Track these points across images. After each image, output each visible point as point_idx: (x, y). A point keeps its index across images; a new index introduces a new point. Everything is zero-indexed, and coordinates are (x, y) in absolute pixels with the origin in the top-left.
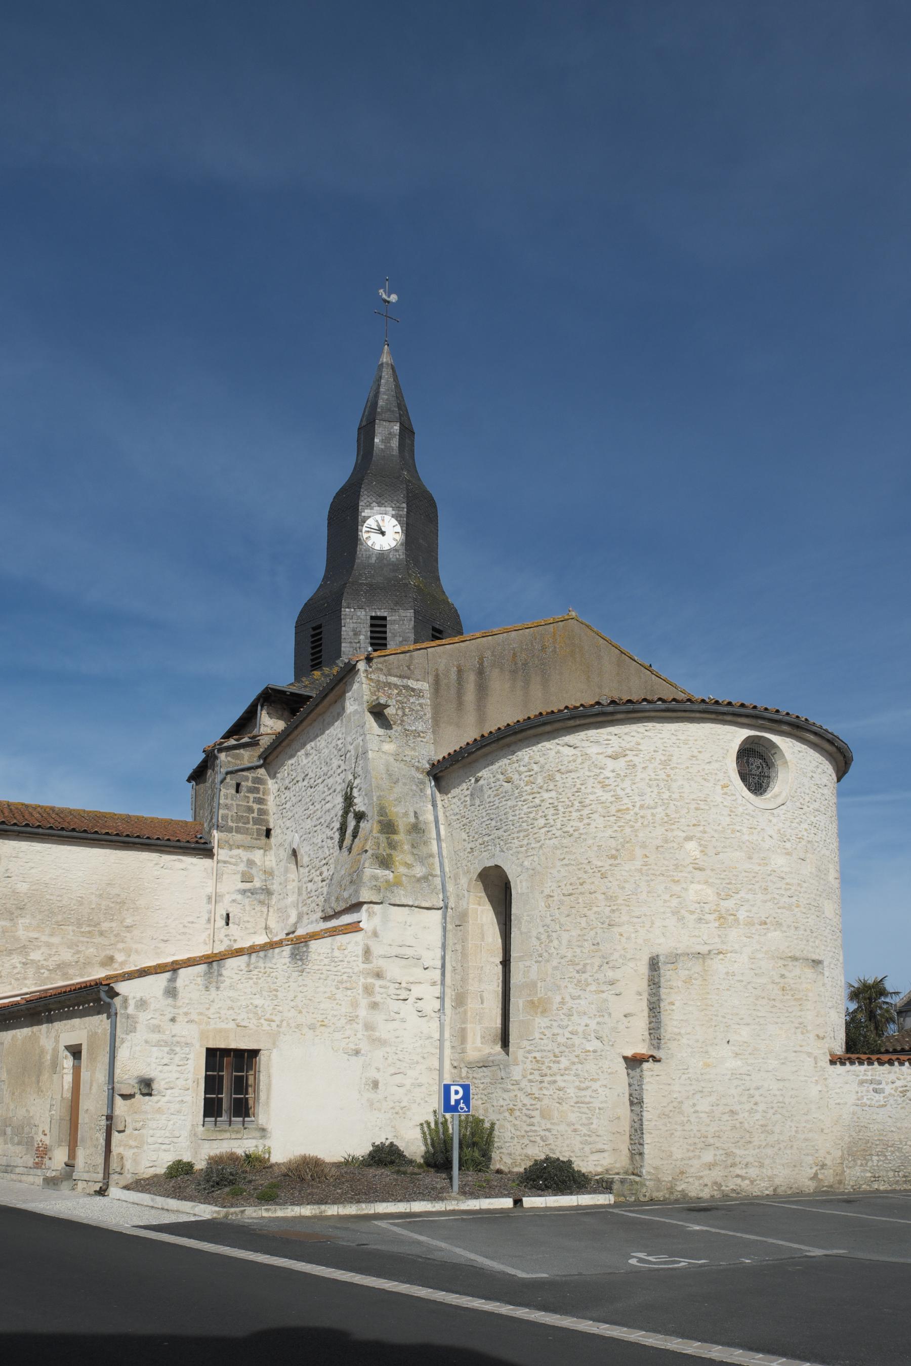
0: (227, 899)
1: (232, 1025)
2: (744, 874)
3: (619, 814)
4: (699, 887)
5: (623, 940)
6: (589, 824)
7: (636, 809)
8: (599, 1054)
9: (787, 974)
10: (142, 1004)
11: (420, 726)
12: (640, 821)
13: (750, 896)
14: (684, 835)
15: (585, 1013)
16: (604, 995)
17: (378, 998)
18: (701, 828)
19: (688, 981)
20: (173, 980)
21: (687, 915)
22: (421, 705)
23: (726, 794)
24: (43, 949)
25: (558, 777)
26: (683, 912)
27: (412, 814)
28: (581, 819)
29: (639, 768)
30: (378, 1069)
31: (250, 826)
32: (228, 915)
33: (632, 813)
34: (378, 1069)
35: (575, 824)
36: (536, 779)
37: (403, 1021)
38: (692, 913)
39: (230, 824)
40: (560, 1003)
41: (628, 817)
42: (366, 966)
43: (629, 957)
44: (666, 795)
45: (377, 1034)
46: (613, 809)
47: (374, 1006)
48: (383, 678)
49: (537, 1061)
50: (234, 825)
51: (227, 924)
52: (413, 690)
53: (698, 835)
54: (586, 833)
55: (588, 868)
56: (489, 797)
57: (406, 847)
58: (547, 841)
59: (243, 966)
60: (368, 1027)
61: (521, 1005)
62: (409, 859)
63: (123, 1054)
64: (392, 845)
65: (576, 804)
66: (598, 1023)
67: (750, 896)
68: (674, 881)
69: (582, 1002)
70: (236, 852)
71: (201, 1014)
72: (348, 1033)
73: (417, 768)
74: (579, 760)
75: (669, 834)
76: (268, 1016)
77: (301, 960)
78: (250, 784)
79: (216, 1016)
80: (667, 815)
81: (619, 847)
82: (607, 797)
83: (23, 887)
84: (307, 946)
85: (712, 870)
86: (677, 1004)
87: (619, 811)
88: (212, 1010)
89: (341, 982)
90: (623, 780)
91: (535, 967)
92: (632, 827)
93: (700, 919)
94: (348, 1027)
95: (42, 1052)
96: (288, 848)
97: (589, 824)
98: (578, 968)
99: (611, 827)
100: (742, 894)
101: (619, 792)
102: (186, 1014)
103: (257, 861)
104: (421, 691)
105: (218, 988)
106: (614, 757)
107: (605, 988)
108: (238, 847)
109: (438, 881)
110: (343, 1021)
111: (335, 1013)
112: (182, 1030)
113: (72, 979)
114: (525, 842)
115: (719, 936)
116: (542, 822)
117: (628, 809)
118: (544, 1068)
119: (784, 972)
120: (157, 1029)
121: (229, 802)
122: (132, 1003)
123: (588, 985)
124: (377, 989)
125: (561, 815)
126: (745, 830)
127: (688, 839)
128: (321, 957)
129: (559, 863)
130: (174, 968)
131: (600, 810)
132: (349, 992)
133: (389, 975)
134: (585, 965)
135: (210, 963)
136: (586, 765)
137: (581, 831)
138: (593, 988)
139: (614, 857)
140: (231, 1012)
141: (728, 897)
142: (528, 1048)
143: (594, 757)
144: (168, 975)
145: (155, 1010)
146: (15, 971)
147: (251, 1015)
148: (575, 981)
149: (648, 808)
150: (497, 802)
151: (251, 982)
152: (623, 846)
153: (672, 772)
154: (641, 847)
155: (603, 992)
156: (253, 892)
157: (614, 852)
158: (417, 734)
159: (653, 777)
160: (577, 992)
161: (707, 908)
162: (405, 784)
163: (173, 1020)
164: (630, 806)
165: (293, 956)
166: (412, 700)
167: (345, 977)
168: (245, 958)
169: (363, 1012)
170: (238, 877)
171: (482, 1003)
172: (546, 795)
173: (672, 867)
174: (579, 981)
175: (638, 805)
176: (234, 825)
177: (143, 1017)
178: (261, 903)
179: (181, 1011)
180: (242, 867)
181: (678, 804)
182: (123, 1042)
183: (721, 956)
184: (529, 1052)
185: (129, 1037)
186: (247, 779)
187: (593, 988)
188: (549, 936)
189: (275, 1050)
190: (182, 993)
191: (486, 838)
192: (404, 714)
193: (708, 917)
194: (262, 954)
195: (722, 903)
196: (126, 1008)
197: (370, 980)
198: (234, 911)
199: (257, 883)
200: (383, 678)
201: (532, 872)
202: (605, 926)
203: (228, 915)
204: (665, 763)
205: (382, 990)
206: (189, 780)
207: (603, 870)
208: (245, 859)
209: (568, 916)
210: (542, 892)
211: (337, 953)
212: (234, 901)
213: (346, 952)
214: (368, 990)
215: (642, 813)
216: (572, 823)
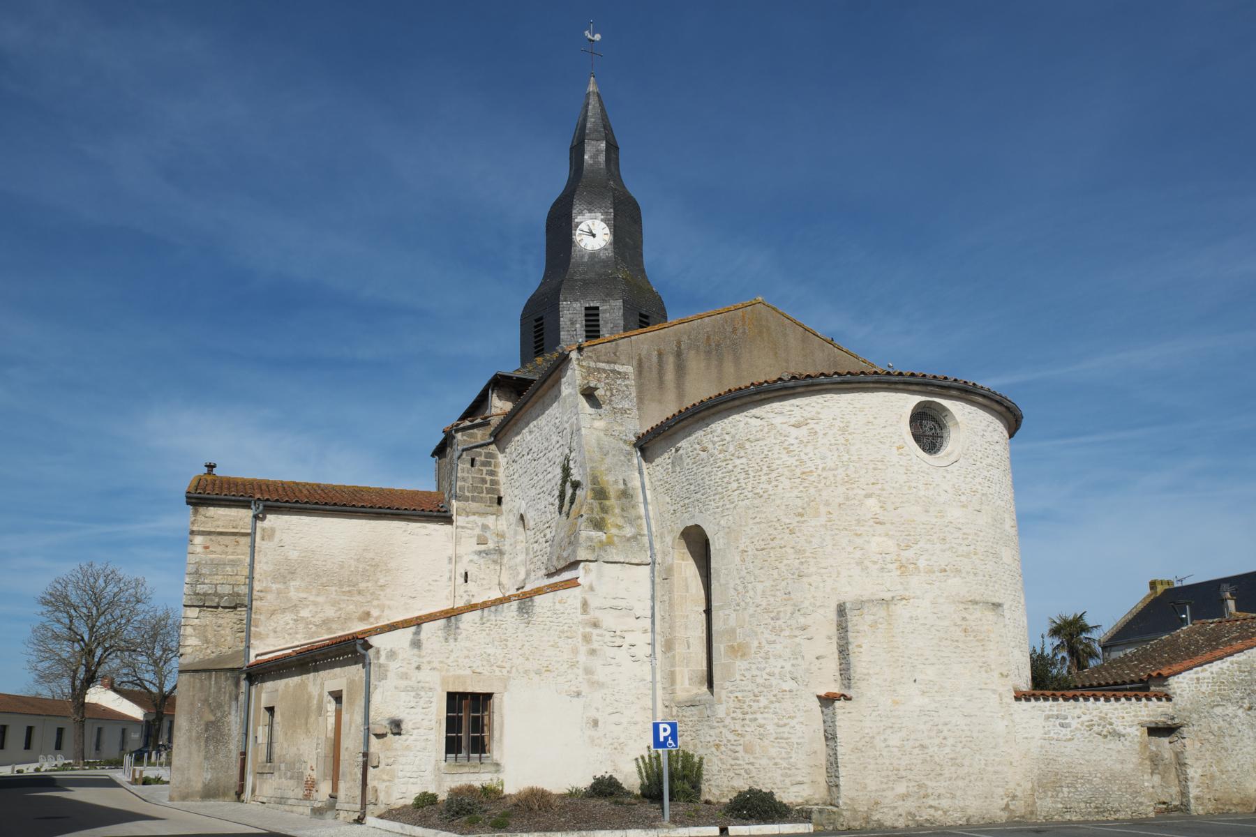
0: (466, 559)
1: (468, 672)
5: (812, 589)
9: (967, 616)
10: (392, 654)
12: (823, 481)
16: (797, 640)
17: (595, 646)
18: (879, 486)
19: (874, 625)
20: (417, 633)
21: (870, 565)
22: (626, 386)
25: (747, 445)
26: (866, 562)
28: (769, 482)
29: (820, 434)
35: (764, 486)
41: (812, 479)
44: (845, 458)
48: (592, 364)
52: (619, 373)
53: (878, 492)
55: (777, 525)
57: (617, 511)
59: (477, 620)
60: (588, 671)
62: (620, 521)
63: (376, 698)
64: (604, 510)
65: (765, 468)
67: (928, 546)
69: (778, 646)
70: (472, 518)
71: (441, 662)
73: (625, 441)
74: (766, 430)
75: (850, 493)
78: (483, 459)
82: (792, 461)
83: (294, 555)
84: (532, 601)
88: (451, 659)
91: (733, 615)
95: (310, 697)
98: (772, 615)
100: (921, 544)
102: (429, 662)
104: (626, 374)
106: (797, 426)
107: (797, 633)
108: (474, 514)
109: (646, 540)
110: (566, 666)
112: (427, 676)
116: (735, 485)
120: (405, 676)
121: (465, 475)
122: (383, 653)
124: (594, 637)
127: (868, 496)
129: (751, 522)
134: (779, 612)
138: (787, 633)
139: (801, 515)
141: (908, 547)
143: (779, 427)
144: (413, 629)
156: (487, 553)
158: (624, 411)
160: (773, 638)
163: (418, 668)
164: (813, 468)
165: (520, 609)
167: (566, 628)
169: (582, 658)
170: (474, 540)
172: (738, 462)
177: (393, 666)
178: (495, 562)
179: (425, 660)
180: (478, 531)
182: (376, 688)
187: (787, 633)
192: (612, 395)
194: (493, 608)
195: (902, 553)
197: (588, 630)
199: (491, 545)
200: (592, 364)
204: (843, 430)
214: (587, 638)
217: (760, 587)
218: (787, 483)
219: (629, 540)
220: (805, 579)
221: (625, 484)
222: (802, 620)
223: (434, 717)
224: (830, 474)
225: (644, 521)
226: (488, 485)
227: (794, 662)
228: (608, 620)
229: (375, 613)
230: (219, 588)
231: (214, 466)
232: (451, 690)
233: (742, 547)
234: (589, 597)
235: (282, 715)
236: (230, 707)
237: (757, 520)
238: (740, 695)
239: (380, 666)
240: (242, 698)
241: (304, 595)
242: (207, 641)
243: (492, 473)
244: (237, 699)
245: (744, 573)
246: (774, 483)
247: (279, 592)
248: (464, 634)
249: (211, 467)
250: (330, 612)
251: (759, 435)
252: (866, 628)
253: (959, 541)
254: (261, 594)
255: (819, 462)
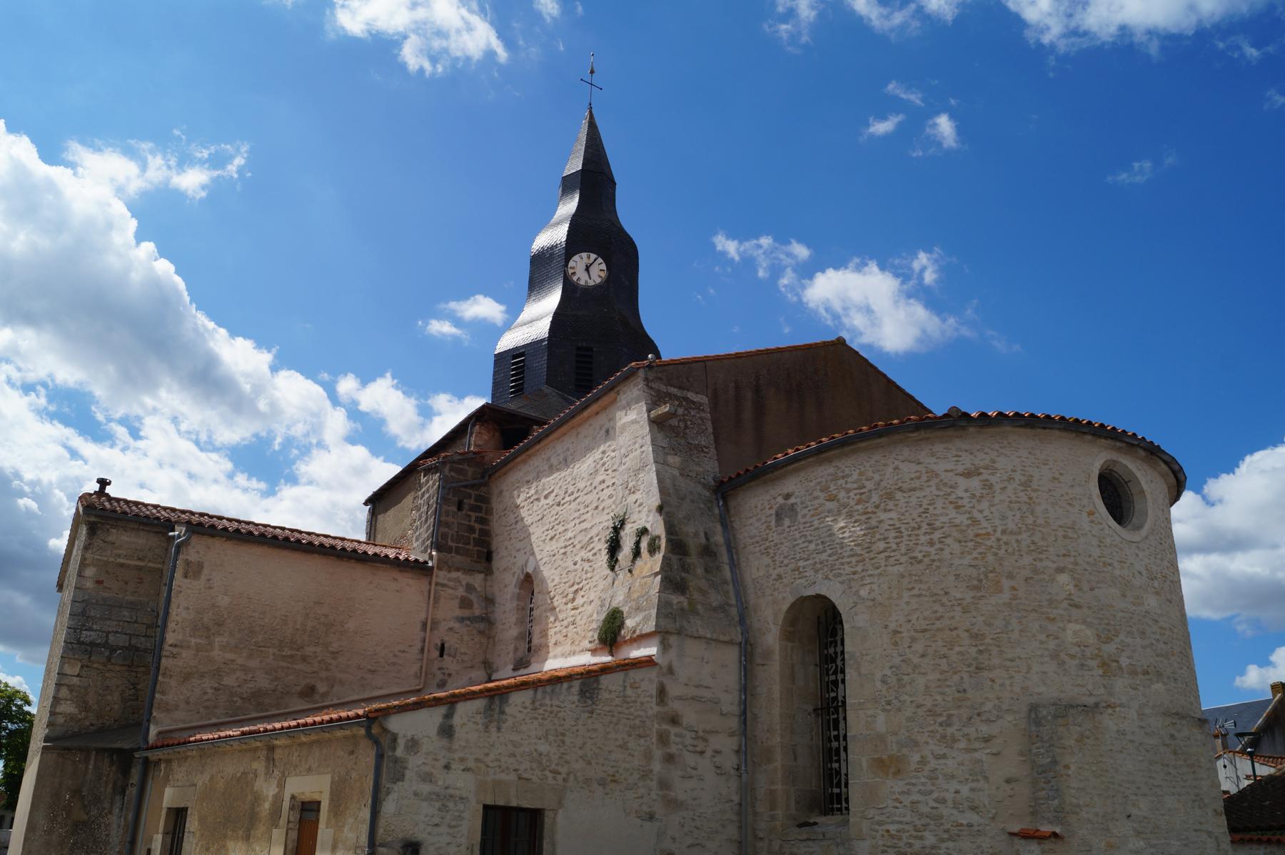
0: (443, 627)
1: (513, 777)
2: (1121, 614)
3: (978, 539)
4: (1078, 627)
5: (996, 687)
6: (942, 550)
7: (998, 534)
8: (976, 828)
9: (1176, 734)
10: (413, 745)
11: (703, 441)
12: (1004, 547)
13: (1129, 640)
14: (1054, 566)
15: (953, 777)
16: (977, 755)
17: (673, 749)
18: (1072, 559)
19: (1081, 739)
20: (449, 716)
21: (1067, 659)
22: (702, 419)
23: (1092, 522)
24: (238, 674)
25: (899, 495)
26: (1063, 656)
27: (702, 535)
28: (931, 543)
29: (997, 487)
30: (674, 839)
31: (471, 547)
32: (443, 645)
33: (993, 538)
34: (674, 839)
35: (924, 548)
36: (870, 497)
37: (701, 779)
38: (1073, 657)
39: (450, 543)
40: (919, 763)
41: (989, 543)
42: (660, 709)
43: (1005, 707)
44: (1030, 520)
45: (672, 794)
46: (971, 533)
47: (669, 759)
48: (663, 388)
49: (892, 836)
50: (454, 545)
51: (441, 655)
52: (693, 403)
53: (1071, 567)
54: (940, 560)
55: (944, 600)
56: (804, 516)
57: (700, 571)
58: (889, 568)
59: (528, 704)
60: (664, 785)
61: (865, 764)
62: (703, 584)
63: (389, 807)
64: (684, 568)
65: (925, 526)
66: (972, 790)
67: (1129, 640)
68: (1048, 618)
69: (950, 762)
70: (454, 575)
71: (478, 760)
72: (642, 791)
73: (704, 486)
74: (924, 478)
75: (1039, 564)
76: (553, 766)
77: (591, 698)
78: (472, 502)
79: (496, 764)
80: (1033, 543)
81: (982, 577)
82: (962, 519)
83: (224, 601)
84: (598, 682)
85: (1089, 608)
86: (1073, 768)
87: (977, 535)
88: (492, 757)
89: (633, 727)
90: (979, 501)
91: (881, 718)
92: (996, 554)
93: (1082, 665)
94: (640, 784)
95: (257, 799)
96: (519, 572)
97: (942, 550)
98: (940, 720)
99: (970, 553)
100: (1122, 637)
101: (976, 515)
102: (462, 760)
103: (477, 586)
104: (701, 404)
105: (499, 729)
106: (968, 474)
107: (977, 745)
108: (458, 570)
109: (734, 611)
110: (636, 776)
111: (627, 766)
112: (461, 782)
113: (267, 710)
114: (859, 568)
115: (1105, 686)
116: (882, 545)
117: (988, 534)
118: (901, 844)
119: (1173, 732)
120: (427, 778)
121: (450, 519)
122: (401, 743)
123: (955, 740)
124: (672, 738)
125: (906, 538)
126: (1116, 564)
127: (1060, 570)
128: (613, 696)
129: (906, 594)
130: (452, 701)
131: (955, 534)
132: (642, 741)
133: (685, 721)
134: (949, 716)
135: (492, 698)
136: (933, 483)
137: (933, 557)
138: (962, 745)
139: (977, 588)
140: (512, 760)
141: (1108, 640)
142: (877, 818)
143: (943, 475)
144: (442, 710)
145: (427, 754)
146: (206, 698)
147: (534, 765)
148: (938, 736)
149: (1011, 533)
150: (816, 523)
151: (536, 723)
152: (986, 577)
153: (1034, 495)
154: (1008, 577)
155: (975, 750)
156: (473, 619)
157: (975, 583)
158: (700, 449)
159: (1014, 498)
160: (941, 750)
161: (1088, 652)
162: (693, 501)
163: (447, 767)
164: (990, 530)
165: (582, 693)
166: (693, 413)
167: (637, 722)
168: (530, 692)
169: (657, 766)
170: (456, 603)
171: (795, 759)
172: (883, 516)
173: (1045, 603)
174: (943, 737)
175: (999, 529)
176: (454, 545)
177: (415, 763)
178: (481, 632)
179: (457, 756)
180: (461, 592)
181: (1044, 530)
182: (388, 793)
183: (1110, 711)
184: (880, 823)
185: (396, 788)
186: (469, 496)
187: (962, 745)
188: (899, 680)
189: (560, 811)
190: (460, 733)
191: (801, 563)
192: (686, 427)
193: (1093, 663)
194: (549, 689)
195: (1104, 647)
196: (394, 749)
197: (665, 727)
198: (451, 641)
199: (477, 611)
200: (663, 388)
201: (871, 603)
202: (972, 669)
203: (443, 645)
204: (1026, 485)
205: (678, 740)
206: (366, 504)
207: (965, 603)
208: (464, 583)
209: (923, 656)
210: (886, 627)
211: (629, 692)
212: (451, 629)
213: (639, 691)
214: (663, 739)
215: (1005, 538)
216: (920, 548)
217: (921, 681)
218: (956, 547)
219: (715, 609)
220: (985, 674)
221: (707, 539)
222: (985, 729)
223: (464, 840)
224: (1012, 539)
225: (731, 588)
226: (476, 535)
227: (974, 785)
228: (690, 716)
229: (322, 688)
230: (111, 638)
231: (109, 483)
232: (489, 802)
233: (893, 626)
234: (667, 682)
235: (202, 820)
236: (112, 804)
237: (916, 592)
238: (892, 828)
239: (396, 760)
240: (132, 792)
241: (229, 656)
242: (85, 708)
243: (483, 521)
244: (123, 792)
245: (897, 661)
246: (938, 546)
247: (199, 648)
248: (510, 723)
249: (103, 483)
250: (263, 682)
251: (917, 484)
252: (1072, 743)
253: (1158, 636)
254: (175, 650)
255: (997, 522)
